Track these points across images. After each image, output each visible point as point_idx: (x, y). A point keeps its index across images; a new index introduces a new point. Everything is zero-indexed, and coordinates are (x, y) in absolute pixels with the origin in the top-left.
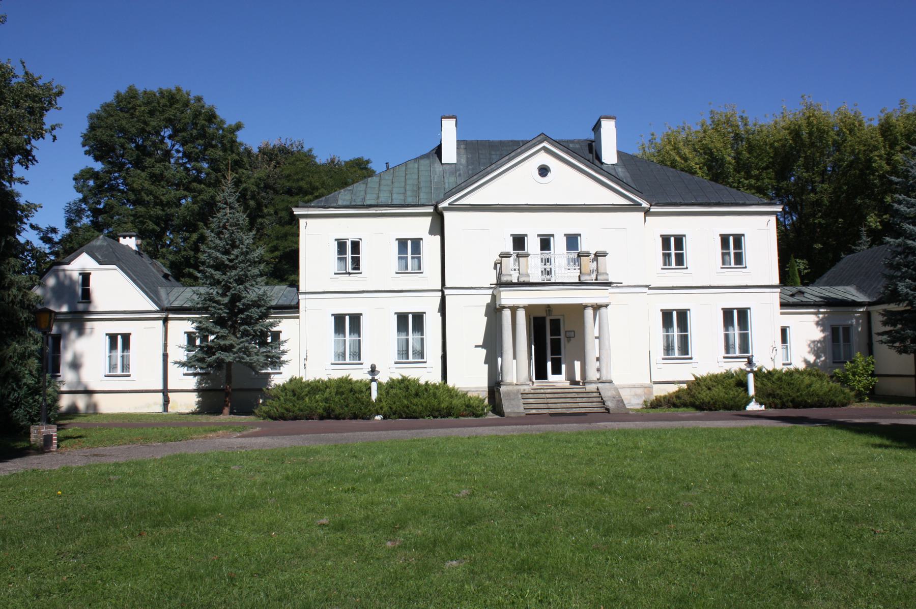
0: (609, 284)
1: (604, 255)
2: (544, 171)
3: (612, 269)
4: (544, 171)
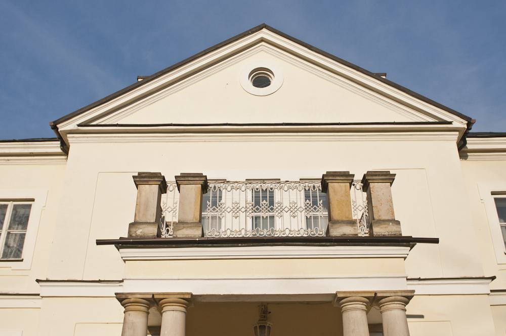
0: (410, 242)
1: (388, 177)
2: (261, 79)
3: (408, 211)
4: (261, 79)
